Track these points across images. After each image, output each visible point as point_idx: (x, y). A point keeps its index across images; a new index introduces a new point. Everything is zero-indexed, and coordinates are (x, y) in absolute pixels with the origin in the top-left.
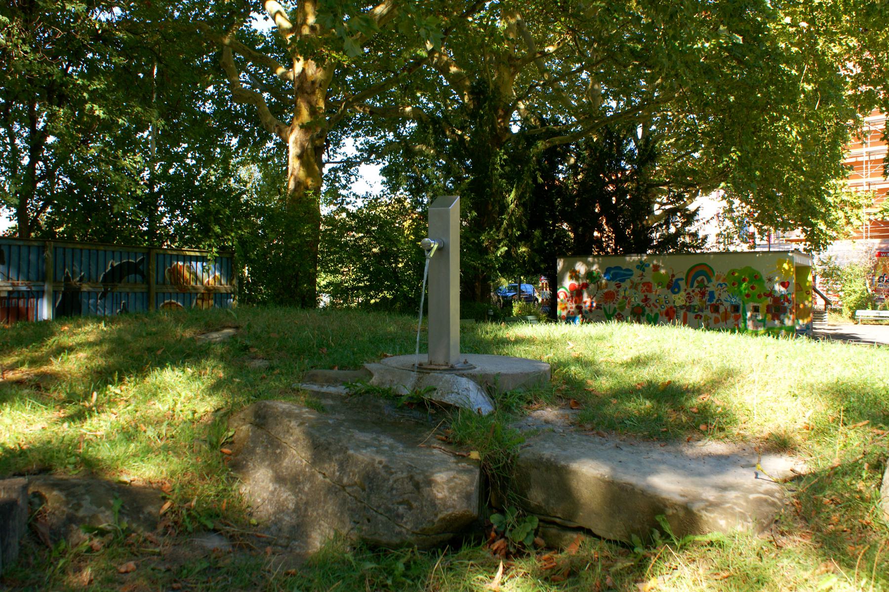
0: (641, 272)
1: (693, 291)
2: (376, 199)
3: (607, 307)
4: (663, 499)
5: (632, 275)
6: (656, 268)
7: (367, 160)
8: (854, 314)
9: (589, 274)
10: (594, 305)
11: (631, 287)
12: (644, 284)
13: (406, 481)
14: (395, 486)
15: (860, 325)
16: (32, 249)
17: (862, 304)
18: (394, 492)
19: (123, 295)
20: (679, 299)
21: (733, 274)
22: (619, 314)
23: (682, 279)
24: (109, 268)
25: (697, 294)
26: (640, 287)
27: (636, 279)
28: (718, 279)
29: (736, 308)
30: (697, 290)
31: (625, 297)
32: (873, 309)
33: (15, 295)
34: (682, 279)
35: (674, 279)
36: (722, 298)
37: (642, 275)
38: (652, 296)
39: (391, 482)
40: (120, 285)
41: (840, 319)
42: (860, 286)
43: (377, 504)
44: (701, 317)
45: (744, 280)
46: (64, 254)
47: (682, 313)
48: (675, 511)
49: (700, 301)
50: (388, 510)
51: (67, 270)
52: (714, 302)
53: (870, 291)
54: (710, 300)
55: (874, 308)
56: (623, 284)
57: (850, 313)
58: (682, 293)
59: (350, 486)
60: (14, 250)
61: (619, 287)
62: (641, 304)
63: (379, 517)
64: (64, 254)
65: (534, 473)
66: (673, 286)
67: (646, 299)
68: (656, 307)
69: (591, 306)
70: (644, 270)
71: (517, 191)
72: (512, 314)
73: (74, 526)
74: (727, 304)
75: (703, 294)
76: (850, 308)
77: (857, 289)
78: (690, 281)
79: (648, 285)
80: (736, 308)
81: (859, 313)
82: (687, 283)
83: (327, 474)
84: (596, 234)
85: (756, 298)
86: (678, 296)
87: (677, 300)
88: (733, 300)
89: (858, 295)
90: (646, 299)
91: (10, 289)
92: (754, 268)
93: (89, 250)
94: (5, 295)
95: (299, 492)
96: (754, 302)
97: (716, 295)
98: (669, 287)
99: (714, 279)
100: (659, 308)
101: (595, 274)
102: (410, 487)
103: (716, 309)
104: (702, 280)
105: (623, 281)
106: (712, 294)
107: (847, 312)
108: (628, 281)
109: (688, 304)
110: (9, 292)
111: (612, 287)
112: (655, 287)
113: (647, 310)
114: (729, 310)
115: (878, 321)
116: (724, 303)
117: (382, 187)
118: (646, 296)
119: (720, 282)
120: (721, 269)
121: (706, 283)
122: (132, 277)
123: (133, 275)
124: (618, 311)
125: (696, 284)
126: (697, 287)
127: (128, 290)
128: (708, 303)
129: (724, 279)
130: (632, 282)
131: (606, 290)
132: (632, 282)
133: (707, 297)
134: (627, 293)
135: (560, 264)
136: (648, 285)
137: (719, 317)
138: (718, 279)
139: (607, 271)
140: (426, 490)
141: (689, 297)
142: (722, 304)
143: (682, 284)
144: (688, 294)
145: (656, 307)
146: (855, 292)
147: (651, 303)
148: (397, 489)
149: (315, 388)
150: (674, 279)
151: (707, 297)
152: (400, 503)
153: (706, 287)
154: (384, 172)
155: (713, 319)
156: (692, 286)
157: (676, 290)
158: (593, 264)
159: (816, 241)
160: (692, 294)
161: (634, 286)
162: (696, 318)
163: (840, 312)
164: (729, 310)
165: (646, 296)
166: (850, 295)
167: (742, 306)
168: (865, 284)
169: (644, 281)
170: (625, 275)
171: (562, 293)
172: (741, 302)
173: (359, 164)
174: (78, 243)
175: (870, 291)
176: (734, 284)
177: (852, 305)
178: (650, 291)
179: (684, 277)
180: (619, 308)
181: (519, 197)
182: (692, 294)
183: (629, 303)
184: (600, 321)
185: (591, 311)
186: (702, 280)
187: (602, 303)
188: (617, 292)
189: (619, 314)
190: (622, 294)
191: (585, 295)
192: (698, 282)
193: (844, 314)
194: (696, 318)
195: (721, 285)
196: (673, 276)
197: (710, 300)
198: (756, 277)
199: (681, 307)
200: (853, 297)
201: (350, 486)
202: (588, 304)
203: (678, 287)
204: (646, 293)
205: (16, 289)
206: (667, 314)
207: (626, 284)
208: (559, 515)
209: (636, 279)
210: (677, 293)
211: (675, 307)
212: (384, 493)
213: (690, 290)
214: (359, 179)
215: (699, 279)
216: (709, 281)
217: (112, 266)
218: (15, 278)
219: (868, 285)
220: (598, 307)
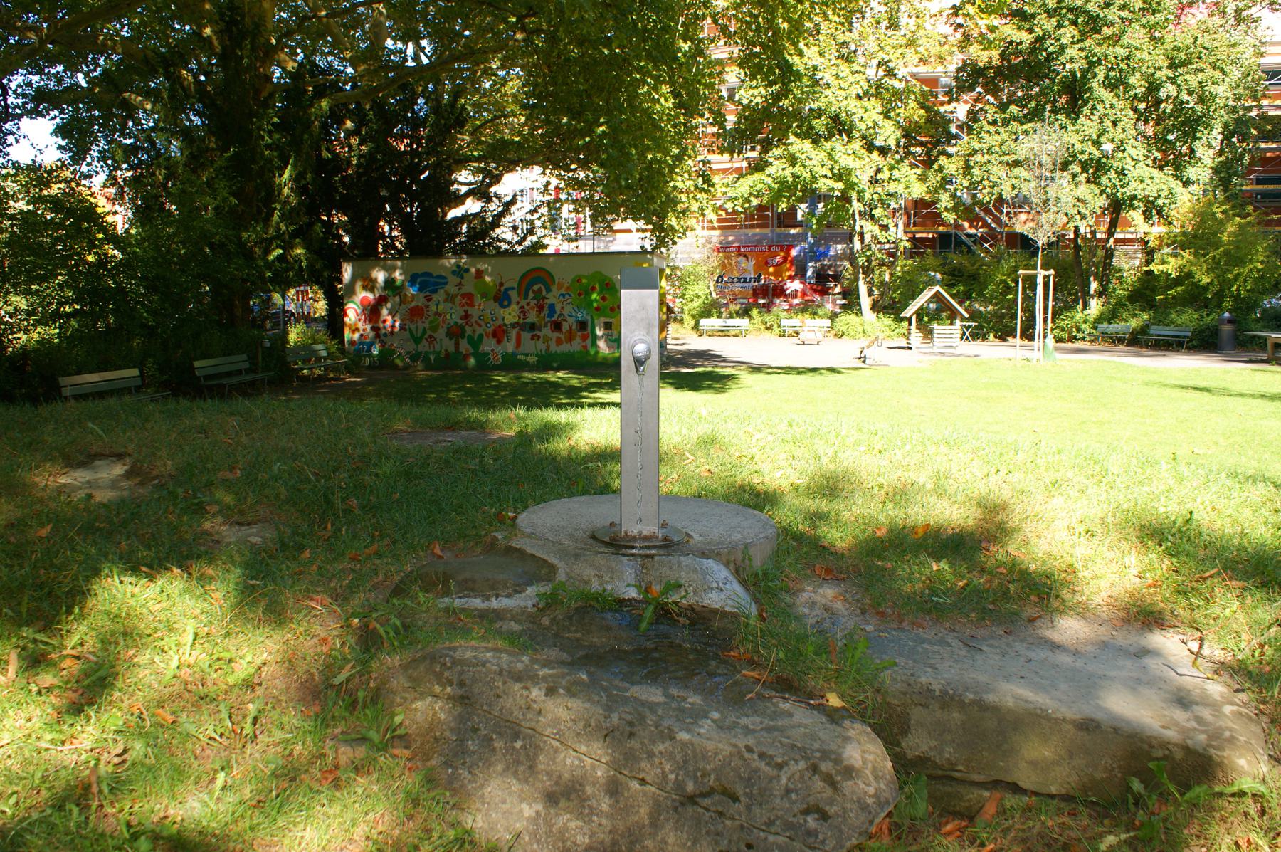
0: (458, 280)
1: (528, 304)
2: (50, 172)
3: (413, 327)
4: (1149, 737)
5: (446, 283)
6: (479, 274)
7: (34, 113)
8: (697, 324)
9: (390, 283)
10: (397, 324)
11: (446, 300)
12: (464, 296)
13: (807, 774)
14: (791, 786)
15: (705, 337)
17: (707, 310)
18: (793, 796)
20: (510, 315)
21: (579, 281)
22: (430, 337)
23: (513, 289)
25: (533, 308)
26: (458, 299)
27: (452, 289)
28: (560, 288)
29: (583, 325)
30: (533, 303)
31: (437, 314)
32: (718, 317)
34: (513, 289)
35: (502, 289)
36: (566, 312)
37: (460, 284)
38: (474, 312)
39: (784, 780)
41: (681, 330)
42: (702, 290)
43: (765, 819)
44: (539, 337)
45: (593, 289)
47: (514, 333)
48: (1167, 752)
49: (538, 316)
50: (789, 826)
52: (555, 318)
53: (714, 295)
54: (550, 315)
55: (719, 316)
56: (435, 297)
57: (693, 322)
58: (514, 306)
59: (703, 795)
61: (429, 300)
62: (460, 322)
63: (771, 838)
65: (916, 713)
66: (502, 298)
67: (466, 316)
68: (480, 326)
69: (393, 326)
70: (462, 277)
71: (295, 166)
72: (288, 342)
74: (571, 321)
75: (541, 308)
76: (693, 316)
77: (700, 294)
78: (523, 289)
79: (469, 297)
80: (583, 325)
81: (703, 322)
82: (519, 294)
83: (648, 778)
85: (608, 311)
86: (507, 311)
87: (507, 317)
88: (579, 315)
89: (701, 301)
90: (466, 316)
92: (603, 272)
95: (591, 813)
96: (605, 316)
97: (558, 309)
98: (496, 299)
99: (554, 288)
100: (484, 327)
101: (398, 283)
103: (557, 326)
104: (540, 290)
105: (435, 291)
106: (552, 307)
107: (689, 322)
108: (441, 291)
109: (521, 321)
111: (421, 301)
112: (478, 299)
113: (468, 330)
114: (574, 327)
115: (723, 332)
116: (568, 318)
117: (58, 155)
118: (466, 312)
119: (563, 291)
120: (563, 276)
121: (544, 293)
124: (429, 332)
125: (531, 295)
126: (534, 298)
128: (547, 319)
129: (568, 288)
130: (447, 294)
131: (413, 304)
132: (447, 294)
133: (546, 312)
134: (441, 308)
135: (347, 272)
136: (469, 297)
137: (562, 336)
138: (560, 288)
139: (413, 279)
140: (848, 785)
141: (523, 312)
142: (565, 320)
143: (514, 295)
144: (522, 307)
145: (480, 326)
146: (698, 297)
147: (473, 320)
148: (796, 791)
149: (477, 603)
150: (502, 289)
151: (546, 312)
152: (806, 812)
153: (544, 298)
154: (60, 131)
155: (554, 339)
156: (526, 298)
157: (506, 303)
158: (394, 268)
159: (664, 236)
160: (527, 308)
161: (450, 298)
162: (532, 338)
163: (681, 321)
164: (574, 327)
165: (466, 312)
166: (692, 301)
167: (589, 324)
168: (709, 288)
169: (462, 291)
170: (437, 284)
171: (353, 313)
172: (589, 318)
173: (19, 117)
175: (714, 295)
176: (580, 294)
177: (695, 312)
178: (471, 305)
179: (515, 285)
180: (430, 328)
181: (297, 179)
182: (527, 308)
183: (443, 321)
185: (392, 333)
186: (540, 290)
187: (408, 322)
188: (427, 306)
189: (430, 337)
190: (434, 308)
191: (385, 312)
192: (534, 292)
193: (686, 324)
194: (532, 338)
195: (563, 295)
196: (501, 284)
197: (550, 315)
198: (607, 284)
199: (513, 326)
200: (697, 303)
201: (703, 795)
202: (388, 324)
203: (509, 298)
204: (466, 308)
206: (495, 335)
207: (439, 296)
208: (960, 768)
209: (452, 289)
210: (505, 307)
211: (505, 325)
212: (778, 801)
213: (523, 303)
214: (21, 140)
215: (536, 287)
216: (549, 290)
219: (712, 289)
220: (402, 328)
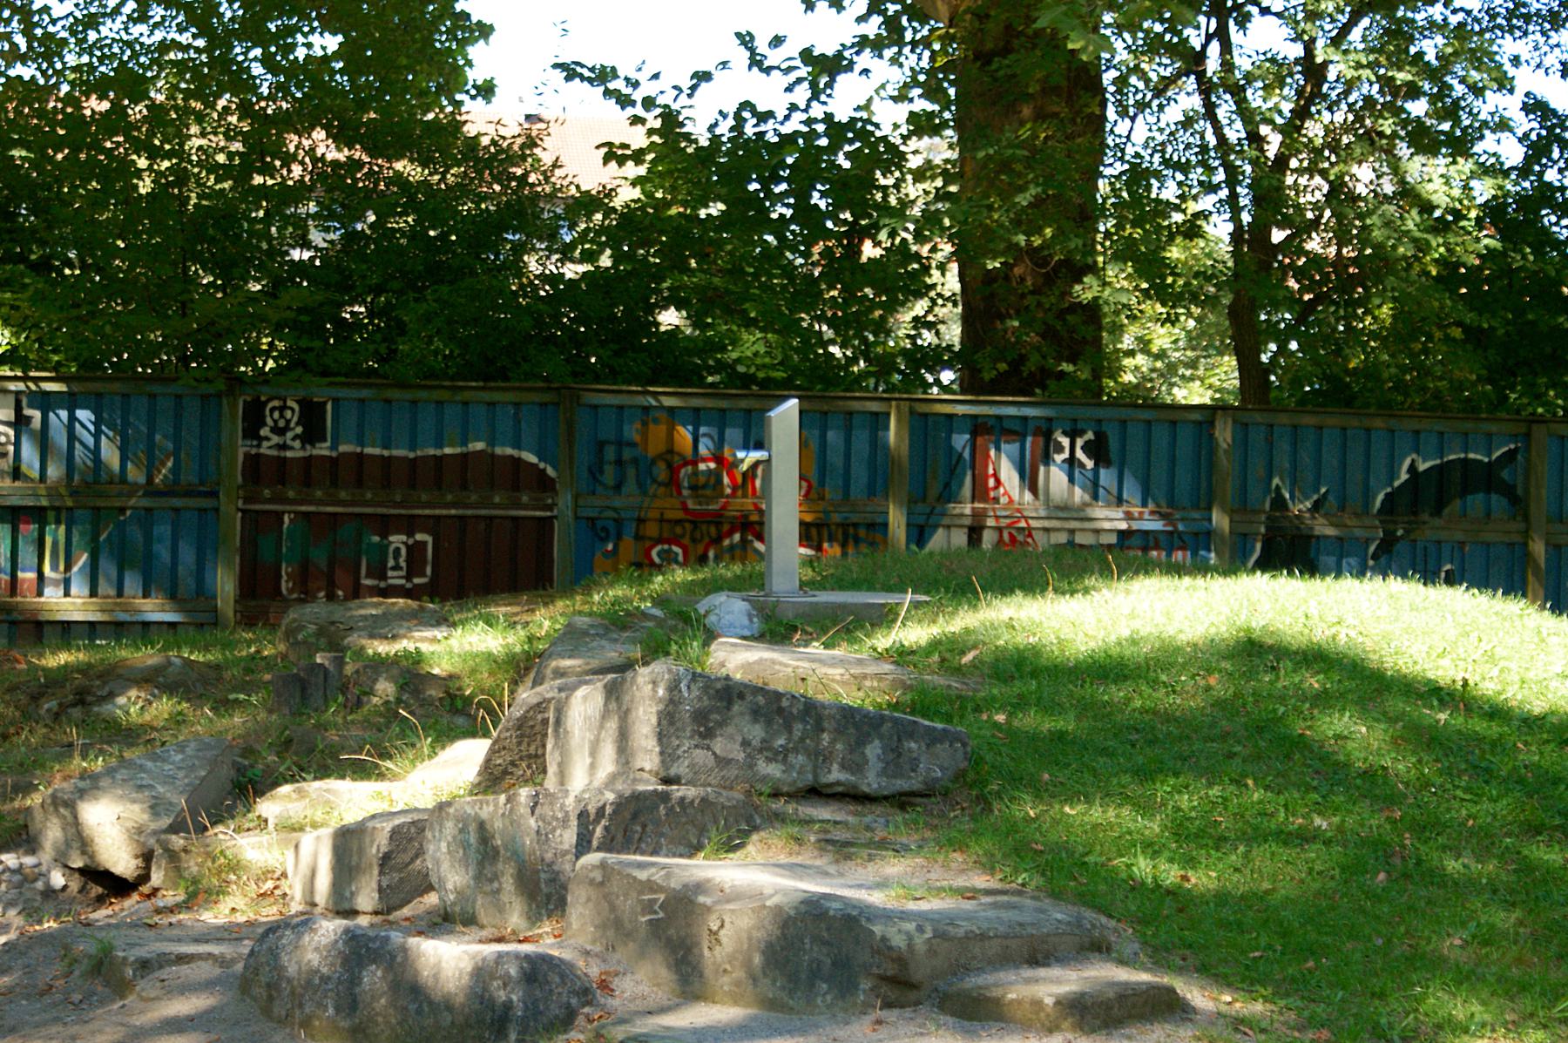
16: (856, 420)
19: (1446, 549)
24: (1404, 476)
33: (1135, 541)
40: (1437, 522)
46: (1270, 443)
51: (1276, 481)
60: (1136, 432)
64: (1270, 443)
73: (325, 970)
84: (318, 263)
91: (1123, 526)
93: (1344, 429)
94: (1113, 539)
102: (555, 1010)
110: (1121, 533)
122: (1476, 501)
123: (1480, 496)
127: (1459, 536)
174: (110, 379)
184: (1137, 573)
205: (1136, 526)
217: (1412, 469)
218: (1137, 500)
